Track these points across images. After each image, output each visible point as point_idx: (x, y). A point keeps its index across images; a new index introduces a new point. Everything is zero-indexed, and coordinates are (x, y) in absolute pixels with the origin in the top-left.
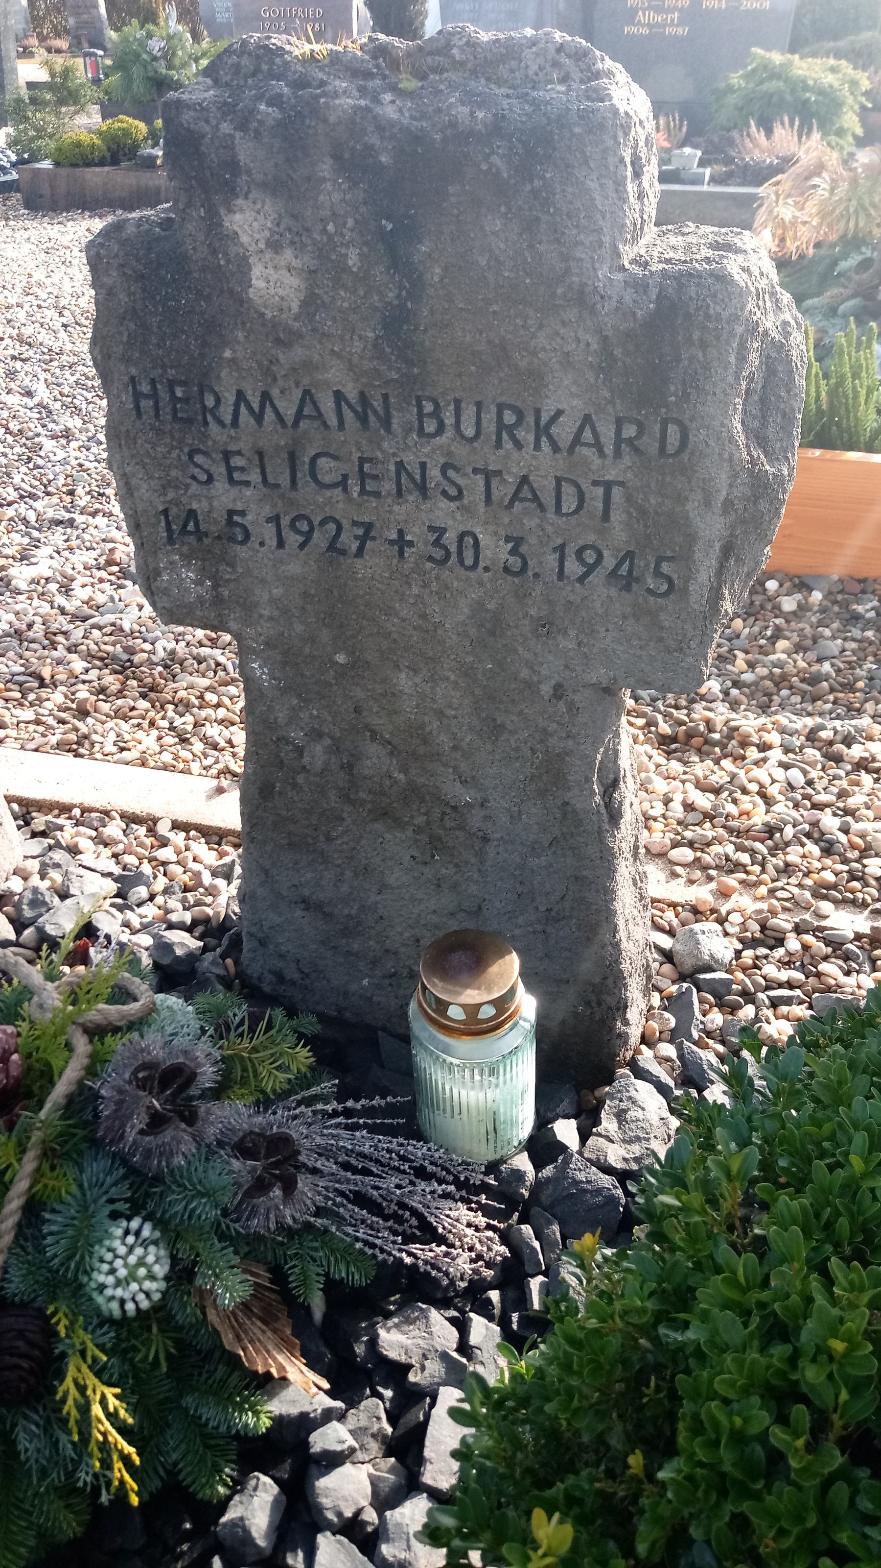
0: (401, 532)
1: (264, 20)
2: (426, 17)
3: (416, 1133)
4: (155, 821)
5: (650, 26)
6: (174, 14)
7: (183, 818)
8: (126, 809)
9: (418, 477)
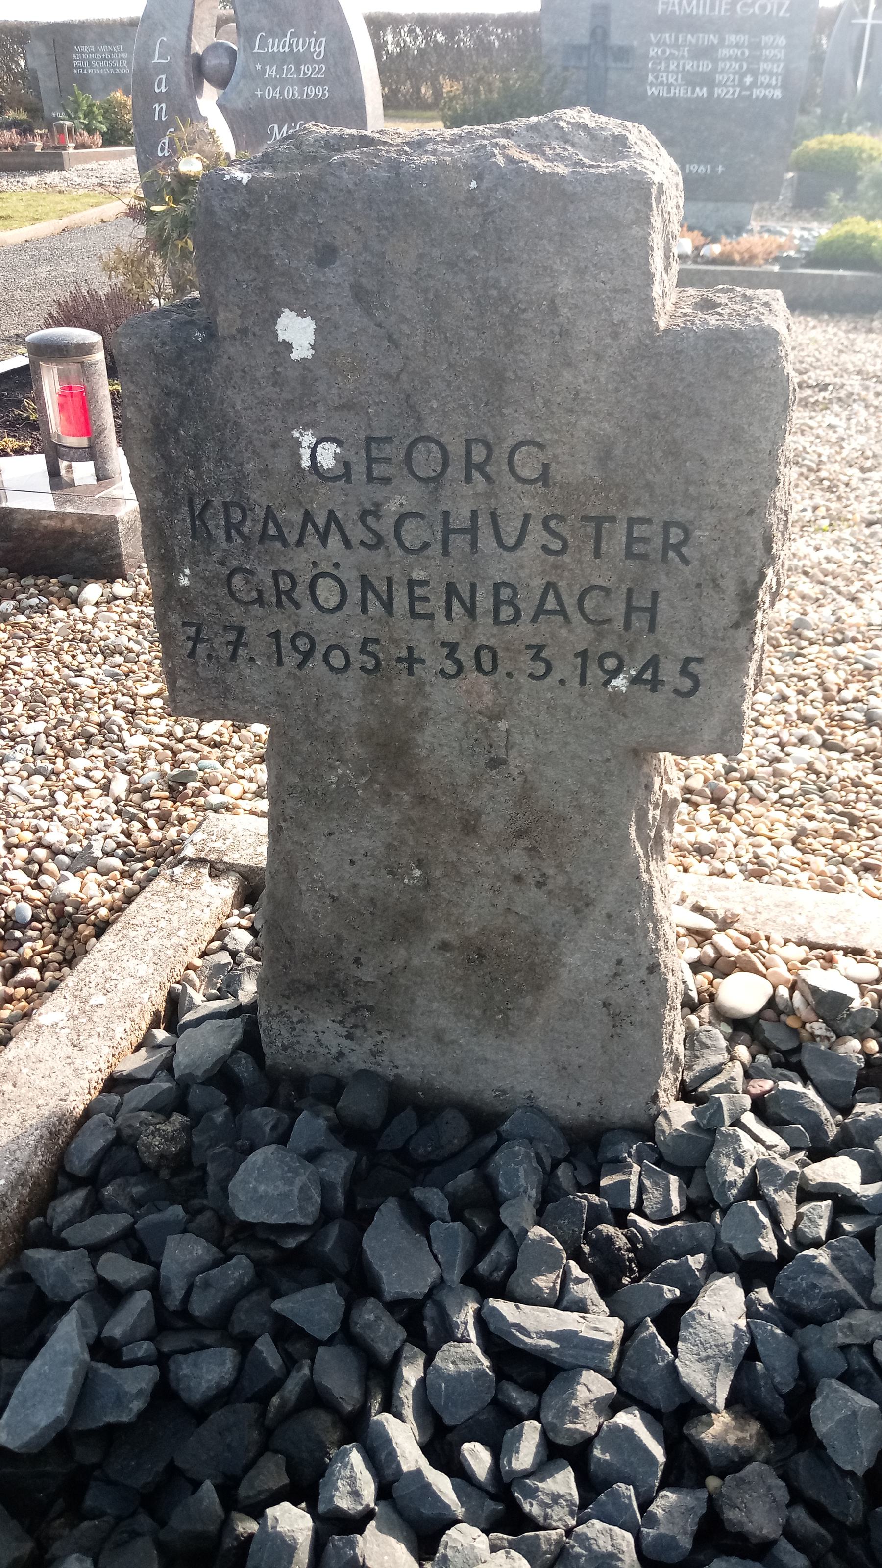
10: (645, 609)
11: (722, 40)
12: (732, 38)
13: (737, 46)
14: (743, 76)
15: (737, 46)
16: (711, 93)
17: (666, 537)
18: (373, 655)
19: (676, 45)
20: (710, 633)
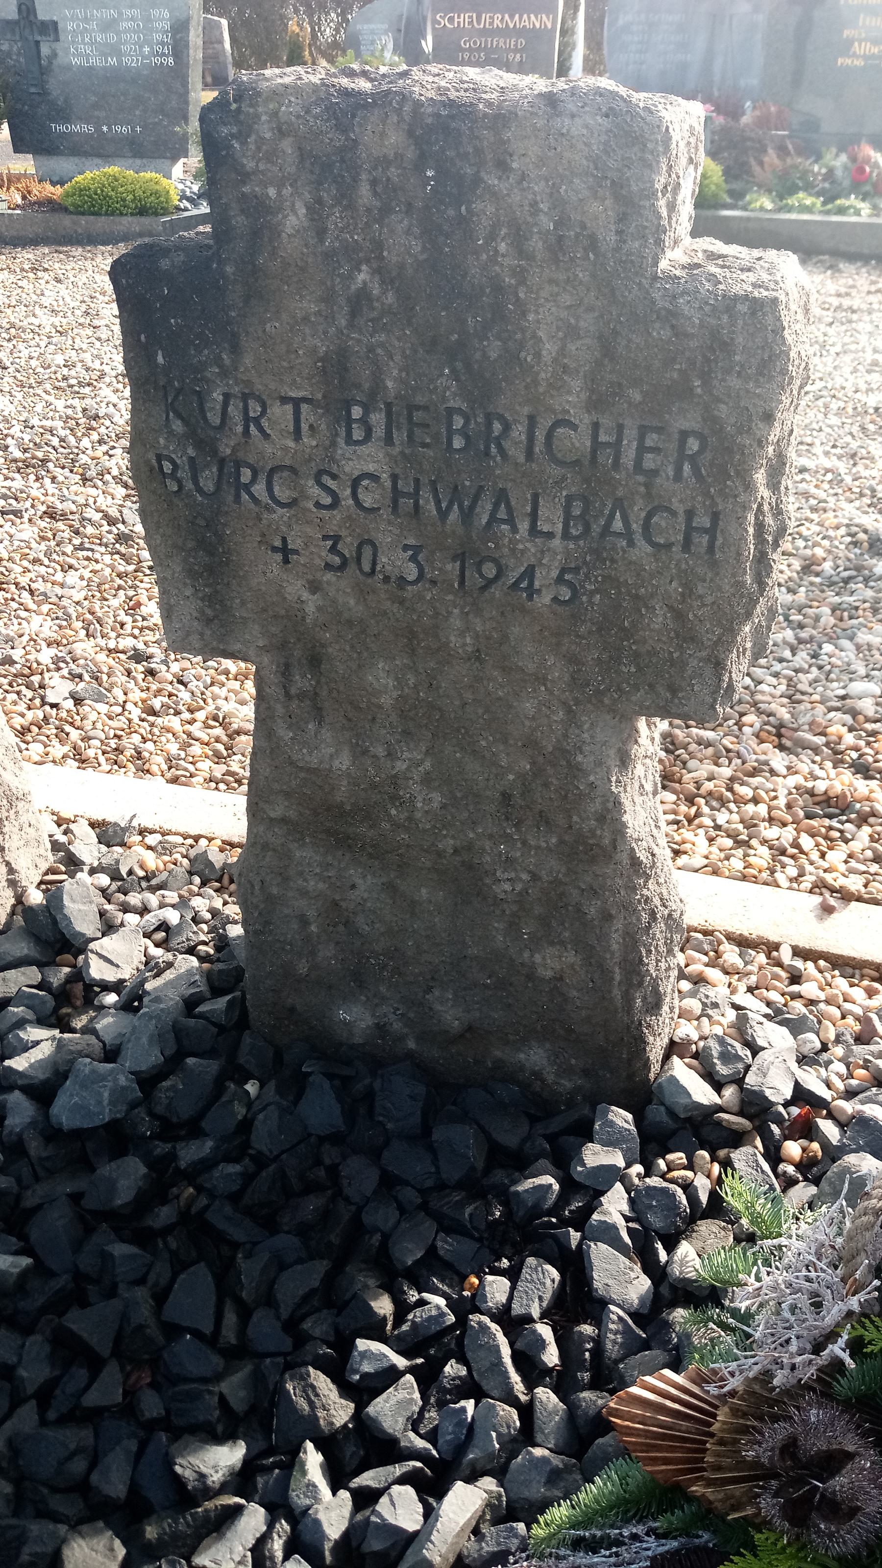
0: (284, 540)
1: (463, 50)
2: (573, 49)
3: (784, 1191)
4: (776, 947)
5: (865, 57)
6: (390, 46)
7: (804, 943)
8: (730, 929)
9: (444, 505)
10: (706, 531)
11: (120, 14)
12: (128, 13)
13: (132, 19)
14: (141, 47)
15: (132, 19)
16: (120, 62)
17: (450, 424)
18: (570, 584)
19: (86, 20)
20: (31, 445)
